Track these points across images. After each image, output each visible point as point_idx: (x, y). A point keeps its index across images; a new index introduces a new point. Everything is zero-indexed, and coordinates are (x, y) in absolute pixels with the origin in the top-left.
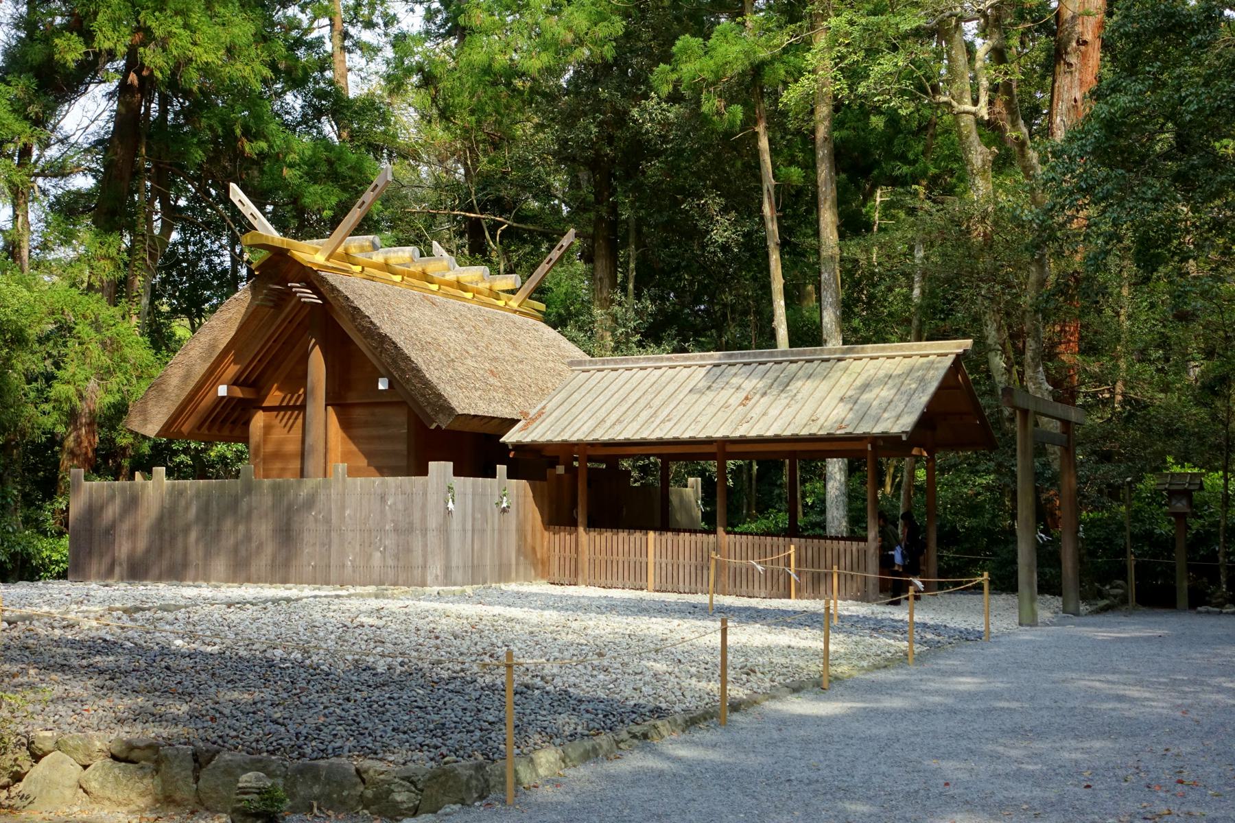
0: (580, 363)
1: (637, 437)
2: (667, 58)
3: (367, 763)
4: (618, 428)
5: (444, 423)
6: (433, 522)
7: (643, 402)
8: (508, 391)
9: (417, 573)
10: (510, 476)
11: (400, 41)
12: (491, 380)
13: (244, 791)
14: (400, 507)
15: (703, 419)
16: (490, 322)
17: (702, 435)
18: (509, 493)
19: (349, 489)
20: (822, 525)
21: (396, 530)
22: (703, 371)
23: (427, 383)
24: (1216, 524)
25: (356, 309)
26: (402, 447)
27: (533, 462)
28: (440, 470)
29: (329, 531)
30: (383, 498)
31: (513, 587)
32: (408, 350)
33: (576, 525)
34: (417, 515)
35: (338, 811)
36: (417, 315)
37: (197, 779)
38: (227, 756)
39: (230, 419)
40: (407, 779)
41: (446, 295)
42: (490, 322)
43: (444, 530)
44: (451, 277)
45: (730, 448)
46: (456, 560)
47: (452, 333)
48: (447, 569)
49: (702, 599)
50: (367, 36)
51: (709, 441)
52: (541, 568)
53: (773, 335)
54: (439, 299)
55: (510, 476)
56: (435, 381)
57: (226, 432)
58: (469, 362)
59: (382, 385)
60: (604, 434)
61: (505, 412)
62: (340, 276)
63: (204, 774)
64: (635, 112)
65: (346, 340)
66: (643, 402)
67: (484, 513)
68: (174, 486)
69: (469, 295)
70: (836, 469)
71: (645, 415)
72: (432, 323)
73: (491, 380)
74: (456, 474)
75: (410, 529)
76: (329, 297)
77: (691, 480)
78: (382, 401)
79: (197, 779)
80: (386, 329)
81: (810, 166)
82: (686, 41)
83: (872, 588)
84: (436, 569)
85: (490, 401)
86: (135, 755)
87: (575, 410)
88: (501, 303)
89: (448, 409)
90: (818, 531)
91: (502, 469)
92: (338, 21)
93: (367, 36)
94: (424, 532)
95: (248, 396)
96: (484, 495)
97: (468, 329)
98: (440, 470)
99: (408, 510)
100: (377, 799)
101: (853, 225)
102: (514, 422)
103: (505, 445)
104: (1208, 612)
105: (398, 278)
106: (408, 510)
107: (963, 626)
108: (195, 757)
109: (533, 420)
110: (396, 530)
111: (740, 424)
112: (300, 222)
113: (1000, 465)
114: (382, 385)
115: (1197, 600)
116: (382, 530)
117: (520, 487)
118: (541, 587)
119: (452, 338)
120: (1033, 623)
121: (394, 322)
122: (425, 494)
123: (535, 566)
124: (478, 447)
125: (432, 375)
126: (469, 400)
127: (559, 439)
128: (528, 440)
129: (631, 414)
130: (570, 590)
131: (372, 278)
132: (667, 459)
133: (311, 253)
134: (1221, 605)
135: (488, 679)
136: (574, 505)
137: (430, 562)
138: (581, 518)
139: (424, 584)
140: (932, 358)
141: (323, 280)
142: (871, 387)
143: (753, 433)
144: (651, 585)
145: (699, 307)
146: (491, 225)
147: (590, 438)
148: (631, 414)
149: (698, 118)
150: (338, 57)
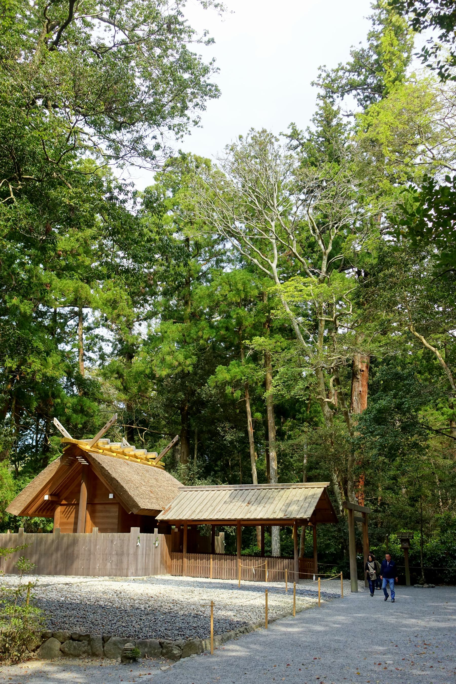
0: (183, 488)
1: (208, 518)
2: (213, 373)
3: (162, 640)
4: (201, 514)
5: (135, 511)
6: (131, 551)
7: (209, 504)
8: (157, 499)
9: (125, 571)
10: (159, 533)
11: (102, 357)
12: (151, 495)
13: (126, 650)
14: (119, 545)
15: (233, 511)
16: (147, 471)
17: (233, 518)
18: (158, 539)
19: (93, 538)
20: (271, 552)
21: (117, 554)
22: (230, 492)
23: (129, 496)
24: (419, 552)
25: (103, 467)
26: (116, 521)
27: (166, 527)
28: (135, 530)
29: (90, 555)
30: (112, 542)
31: (159, 577)
32: (122, 483)
33: (181, 551)
34: (125, 549)
35: (154, 658)
36: (123, 469)
37: (103, 647)
38: (114, 638)
39: (47, 509)
40: (177, 645)
41: (131, 461)
42: (147, 471)
43: (136, 554)
44: (132, 453)
45: (242, 523)
46: (139, 566)
47: (135, 476)
48: (137, 569)
49: (235, 582)
50: (90, 354)
51: (235, 520)
52: (170, 570)
53: (251, 476)
54: (129, 462)
55: (159, 533)
56: (132, 496)
57: (44, 513)
58: (143, 488)
59: (111, 496)
60: (195, 517)
61: (157, 507)
62: (96, 454)
63: (106, 645)
64: (199, 391)
65: (95, 478)
66: (209, 504)
67: (150, 547)
68: (37, 537)
69: (139, 460)
70: (275, 530)
71: (210, 509)
72: (129, 472)
73: (151, 495)
74: (141, 532)
75: (122, 554)
76: (92, 463)
77: (221, 533)
78: (111, 503)
79: (103, 647)
80: (114, 475)
81: (264, 412)
82: (220, 368)
83: (296, 577)
84: (132, 570)
85: (152, 503)
86: (81, 638)
87: (183, 507)
88: (150, 463)
89: (136, 505)
90: (269, 554)
91: (156, 530)
92: (81, 350)
93: (90, 354)
94: (128, 555)
95: (54, 499)
96: (150, 540)
97: (140, 472)
98: (135, 530)
99: (122, 546)
100: (167, 653)
101: (280, 435)
102: (160, 511)
103: (157, 520)
104: (418, 587)
105: (115, 454)
106: (122, 546)
107: (332, 592)
108: (103, 638)
109: (167, 511)
110: (117, 554)
111: (247, 513)
112: (78, 433)
113: (339, 529)
114: (111, 496)
115: (414, 582)
116: (111, 554)
117: (162, 536)
118: (168, 577)
119: (136, 478)
120: (357, 591)
121: (117, 472)
122: (129, 540)
123: (166, 568)
124: (148, 522)
125: (131, 493)
126: (145, 503)
127: (178, 518)
128: (166, 518)
129: (205, 509)
130: (181, 578)
131: (105, 455)
132: (213, 526)
133: (85, 444)
134: (423, 584)
135: (182, 612)
136: (181, 543)
137: (130, 567)
138: (185, 550)
139: (127, 576)
140: (316, 489)
141: (90, 456)
142: (297, 500)
143: (252, 517)
144: (211, 577)
145: (219, 462)
146: (136, 429)
147: (190, 518)
148: (205, 509)
149: (223, 394)
150: (81, 363)
